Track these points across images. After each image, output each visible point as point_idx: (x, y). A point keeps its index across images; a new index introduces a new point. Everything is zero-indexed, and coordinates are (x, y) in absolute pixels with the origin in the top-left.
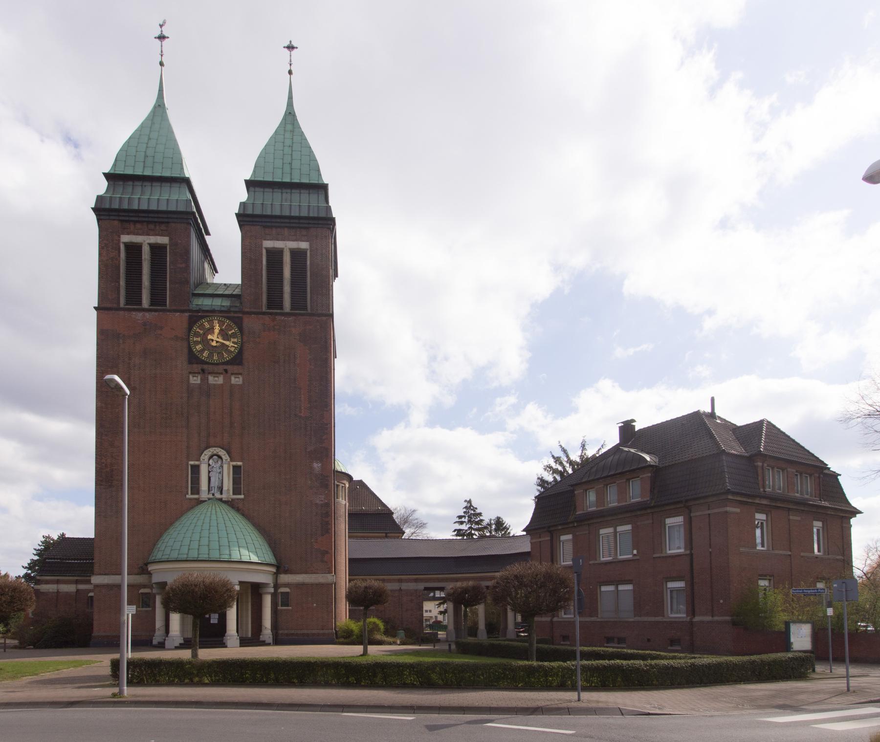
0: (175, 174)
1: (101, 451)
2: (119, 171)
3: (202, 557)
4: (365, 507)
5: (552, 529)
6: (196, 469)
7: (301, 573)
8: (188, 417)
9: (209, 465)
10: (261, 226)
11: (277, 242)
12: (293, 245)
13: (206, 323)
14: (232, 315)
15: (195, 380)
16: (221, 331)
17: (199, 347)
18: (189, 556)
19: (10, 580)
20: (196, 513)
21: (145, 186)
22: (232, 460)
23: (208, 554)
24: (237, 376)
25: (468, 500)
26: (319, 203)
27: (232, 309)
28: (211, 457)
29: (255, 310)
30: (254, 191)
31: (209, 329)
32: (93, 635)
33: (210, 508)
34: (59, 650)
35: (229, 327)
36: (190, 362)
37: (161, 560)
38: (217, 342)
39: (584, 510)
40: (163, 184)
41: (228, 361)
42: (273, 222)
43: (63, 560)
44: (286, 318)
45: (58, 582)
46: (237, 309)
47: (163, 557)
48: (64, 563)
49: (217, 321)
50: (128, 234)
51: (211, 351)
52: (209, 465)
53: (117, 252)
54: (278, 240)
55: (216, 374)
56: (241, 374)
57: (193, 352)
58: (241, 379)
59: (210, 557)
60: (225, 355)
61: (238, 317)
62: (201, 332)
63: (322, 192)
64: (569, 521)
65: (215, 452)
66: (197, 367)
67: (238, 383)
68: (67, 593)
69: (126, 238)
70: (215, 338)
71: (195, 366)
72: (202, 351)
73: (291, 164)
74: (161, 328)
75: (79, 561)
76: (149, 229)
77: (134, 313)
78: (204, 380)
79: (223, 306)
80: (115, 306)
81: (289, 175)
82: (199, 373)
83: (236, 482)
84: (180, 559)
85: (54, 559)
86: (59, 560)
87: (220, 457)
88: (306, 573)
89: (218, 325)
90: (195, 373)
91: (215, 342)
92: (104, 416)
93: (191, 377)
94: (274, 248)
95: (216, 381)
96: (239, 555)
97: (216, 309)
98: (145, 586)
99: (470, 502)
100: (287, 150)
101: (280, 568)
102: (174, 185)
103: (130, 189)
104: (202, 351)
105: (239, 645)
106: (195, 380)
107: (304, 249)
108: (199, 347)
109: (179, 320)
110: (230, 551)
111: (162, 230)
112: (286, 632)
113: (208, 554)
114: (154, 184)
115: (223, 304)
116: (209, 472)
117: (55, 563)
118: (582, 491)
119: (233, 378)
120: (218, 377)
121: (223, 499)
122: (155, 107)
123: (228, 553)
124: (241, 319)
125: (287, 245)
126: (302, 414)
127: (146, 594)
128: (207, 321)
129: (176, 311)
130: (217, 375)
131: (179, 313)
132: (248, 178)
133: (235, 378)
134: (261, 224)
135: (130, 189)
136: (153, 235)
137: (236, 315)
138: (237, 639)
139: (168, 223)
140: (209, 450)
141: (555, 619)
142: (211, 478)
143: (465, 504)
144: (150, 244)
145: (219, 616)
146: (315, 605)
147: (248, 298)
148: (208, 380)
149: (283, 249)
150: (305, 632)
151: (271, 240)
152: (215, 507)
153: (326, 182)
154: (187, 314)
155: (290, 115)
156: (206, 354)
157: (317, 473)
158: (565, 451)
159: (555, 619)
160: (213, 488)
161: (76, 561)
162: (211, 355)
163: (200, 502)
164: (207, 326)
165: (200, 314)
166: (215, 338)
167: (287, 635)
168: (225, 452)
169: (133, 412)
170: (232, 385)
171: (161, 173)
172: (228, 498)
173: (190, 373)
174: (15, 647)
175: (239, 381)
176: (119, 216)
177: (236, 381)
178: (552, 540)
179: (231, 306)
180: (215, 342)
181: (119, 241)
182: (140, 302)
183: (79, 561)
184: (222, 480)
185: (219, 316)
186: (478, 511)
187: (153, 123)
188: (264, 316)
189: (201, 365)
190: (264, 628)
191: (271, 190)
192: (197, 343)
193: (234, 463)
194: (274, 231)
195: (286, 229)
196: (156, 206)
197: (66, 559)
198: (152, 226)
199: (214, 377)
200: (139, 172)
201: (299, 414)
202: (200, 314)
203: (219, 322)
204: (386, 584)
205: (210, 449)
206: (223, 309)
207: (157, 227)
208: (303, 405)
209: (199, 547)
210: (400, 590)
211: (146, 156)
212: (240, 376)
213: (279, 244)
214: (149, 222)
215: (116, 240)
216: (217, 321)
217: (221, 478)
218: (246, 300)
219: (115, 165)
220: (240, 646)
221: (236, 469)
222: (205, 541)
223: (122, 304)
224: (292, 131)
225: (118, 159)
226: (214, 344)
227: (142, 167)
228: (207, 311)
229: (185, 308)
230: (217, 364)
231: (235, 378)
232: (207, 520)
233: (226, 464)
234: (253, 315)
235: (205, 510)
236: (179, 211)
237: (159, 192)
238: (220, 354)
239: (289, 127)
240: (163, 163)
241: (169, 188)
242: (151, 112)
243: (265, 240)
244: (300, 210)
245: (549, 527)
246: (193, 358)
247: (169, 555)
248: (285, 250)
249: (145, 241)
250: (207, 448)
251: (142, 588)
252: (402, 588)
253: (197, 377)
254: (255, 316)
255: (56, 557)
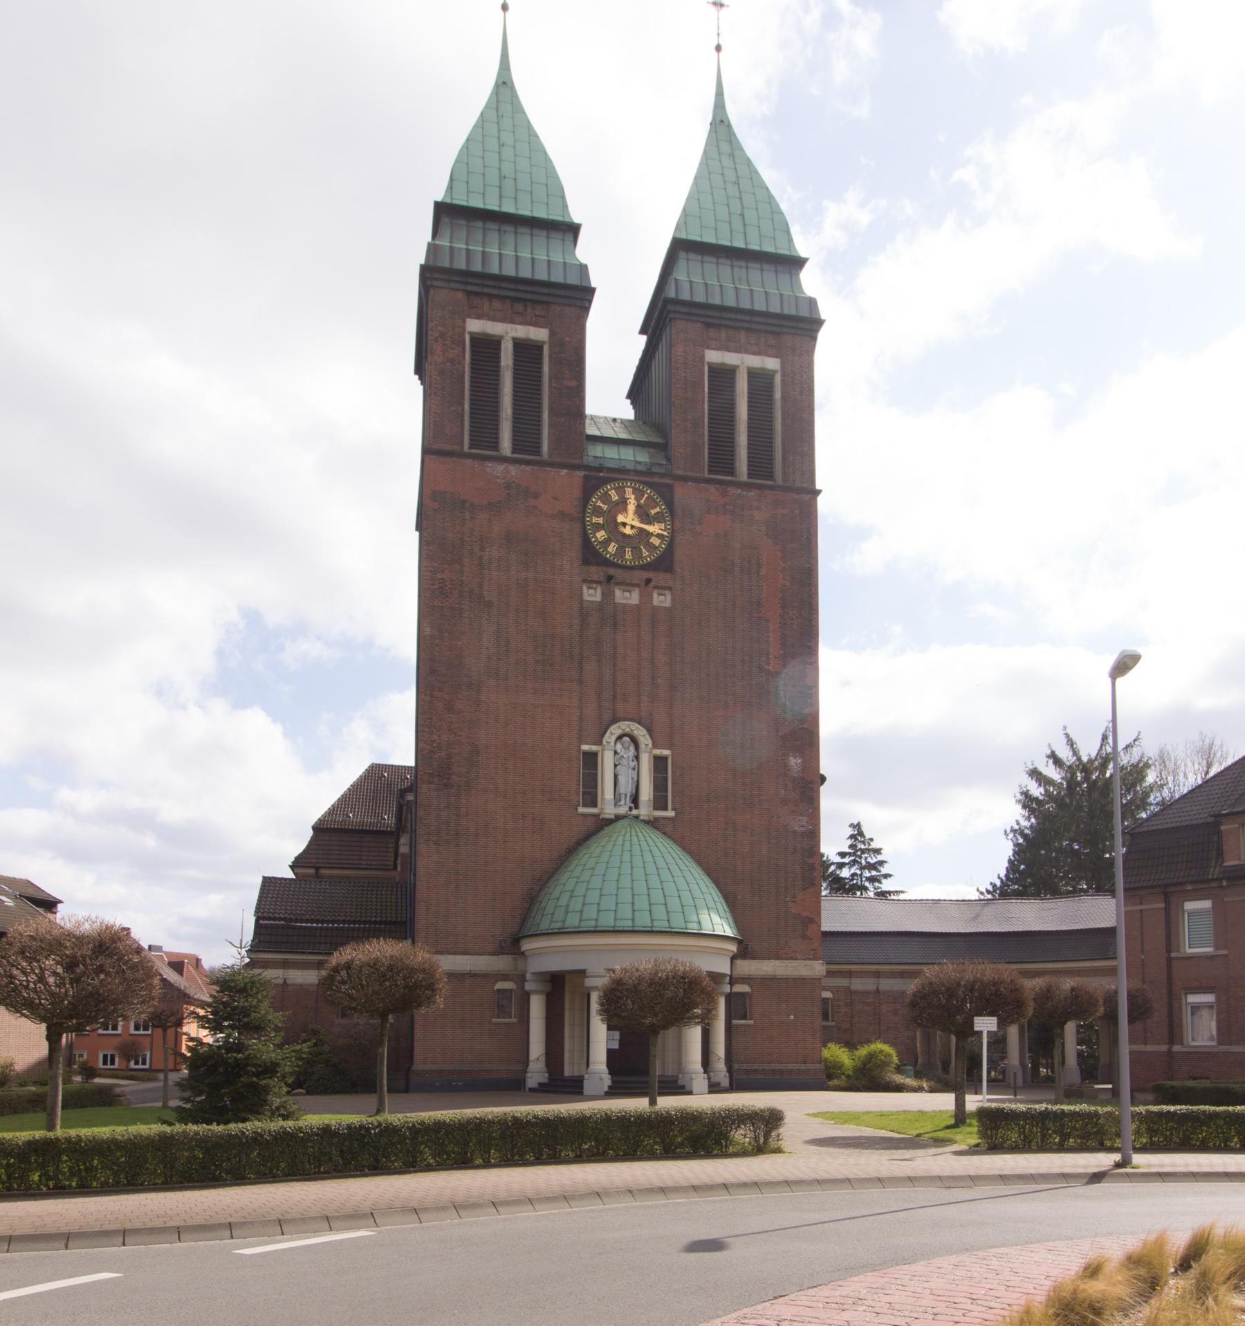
0: (556, 216)
1: (431, 719)
2: (460, 200)
3: (623, 924)
4: (353, 816)
5: (1171, 889)
6: (591, 760)
7: (769, 958)
8: (581, 663)
9: (616, 753)
10: (702, 322)
11: (728, 353)
12: (754, 361)
13: (613, 491)
14: (656, 479)
15: (591, 595)
16: (639, 507)
17: (601, 535)
18: (599, 924)
19: (681, 969)
20: (603, 843)
21: (505, 232)
22: (655, 746)
23: (633, 920)
24: (662, 592)
25: (856, 823)
26: (535, 252)
27: (655, 469)
28: (620, 738)
29: (692, 474)
30: (688, 260)
31: (617, 504)
32: (414, 1068)
33: (628, 834)
34: (553, 1096)
35: (652, 502)
36: (586, 562)
37: (580, 929)
38: (632, 527)
39: (1239, 860)
40: (536, 231)
41: (649, 564)
42: (723, 318)
43: (291, 922)
44: (745, 493)
45: (285, 965)
46: (662, 471)
47: (583, 924)
48: (294, 928)
49: (631, 490)
50: (479, 317)
51: (621, 544)
52: (616, 753)
53: (460, 349)
54: (729, 350)
55: (628, 585)
56: (670, 589)
57: (591, 543)
58: (669, 597)
59: (673, 925)
60: (645, 553)
61: (666, 485)
62: (605, 507)
63: (570, 237)
64: (1210, 877)
65: (628, 730)
66: (596, 572)
67: (664, 605)
68: (301, 986)
69: (475, 325)
70: (629, 519)
71: (593, 568)
72: (606, 543)
73: (742, 215)
74: (536, 496)
75: (320, 925)
76: (515, 313)
77: (490, 465)
78: (608, 595)
79: (640, 463)
80: (456, 448)
81: (742, 236)
82: (599, 582)
83: (660, 787)
84: (621, 929)
85: (275, 919)
86: (282, 922)
87: (634, 740)
88: (778, 958)
89: (633, 497)
90: (592, 582)
91: (628, 528)
92: (437, 654)
93: (585, 588)
94: (723, 364)
95: (626, 598)
96: (683, 921)
97: (628, 468)
98: (505, 977)
99: (857, 827)
100: (733, 191)
101: (744, 951)
102: (554, 235)
103: (479, 235)
104: (606, 543)
105: (707, 1090)
106: (593, 595)
107: (732, 366)
108: (601, 535)
109: (566, 483)
110: (698, 915)
111: (536, 316)
112: (745, 1066)
113: (633, 920)
114: (521, 230)
115: (639, 459)
116: (616, 766)
117: (277, 926)
118: (1238, 825)
119: (655, 595)
120: (630, 592)
121: (642, 818)
122: (497, 86)
123: (696, 919)
124: (670, 488)
125: (743, 361)
126: (770, 668)
127: (505, 991)
128: (615, 489)
129: (562, 466)
130: (629, 588)
131: (566, 471)
132: (439, 199)
133: (659, 594)
134: (703, 319)
135: (479, 235)
136: (521, 323)
137: (662, 481)
138: (725, 1076)
139: (548, 303)
140: (617, 725)
141: (1176, 1048)
142: (619, 777)
143: (850, 831)
144: (514, 339)
145: (621, 1036)
146: (792, 1017)
147: (681, 450)
148: (614, 596)
149: (737, 367)
150: (777, 1066)
151: (718, 350)
152: (636, 832)
153: (576, 220)
154: (581, 473)
155: (504, 84)
156: (612, 548)
157: (796, 775)
158: (1071, 743)
159: (1176, 1048)
160: (623, 796)
161: (315, 925)
162: (621, 551)
163: (602, 824)
164: (615, 497)
165: (601, 474)
166: (629, 519)
167: (747, 1072)
168: (644, 732)
169: (487, 648)
170: (655, 610)
171: (467, 201)
172: (649, 816)
173: (585, 581)
174: (304, 1095)
175: (665, 602)
176: (466, 283)
177: (661, 600)
178: (1167, 910)
179: (652, 464)
180: (628, 528)
181: (464, 328)
182: (495, 445)
183: (320, 925)
184: (638, 781)
185: (633, 480)
186: (874, 845)
187: (500, 117)
188: (708, 486)
189: (604, 568)
190: (716, 1060)
191: (714, 260)
192: (598, 527)
193: (657, 752)
194: (723, 334)
195: (743, 333)
196: (765, 304)
197: (297, 920)
198: (519, 307)
199: (624, 591)
200: (493, 205)
201: (766, 667)
202: (601, 474)
203: (635, 491)
204: (854, 980)
205: (620, 724)
206: (639, 468)
207: (529, 310)
208: (772, 651)
209: (582, 908)
210: (878, 991)
211: (502, 178)
212: (667, 592)
213: (731, 358)
214: (515, 300)
215: (460, 327)
216: (631, 490)
217: (636, 779)
218: (678, 454)
219: (450, 187)
220: (710, 1092)
221: (659, 763)
222: (626, 896)
223: (466, 448)
224: (732, 155)
225: (454, 177)
226: (628, 531)
227: (498, 197)
228: (610, 470)
229: (577, 461)
230: (632, 568)
231: (589, 588)
232: (627, 856)
233: (646, 752)
234: (690, 483)
235: (621, 838)
236: (681, 300)
237: (513, 245)
238: (636, 550)
239: (725, 147)
240: (531, 192)
241: (545, 239)
242: (492, 93)
243: (708, 348)
244: (767, 300)
245: (1166, 886)
246: (591, 555)
247: (596, 920)
248: (741, 368)
249: (507, 333)
250: (615, 721)
251: (501, 980)
252: (880, 988)
253: (595, 589)
254: (694, 484)
255: (277, 916)
